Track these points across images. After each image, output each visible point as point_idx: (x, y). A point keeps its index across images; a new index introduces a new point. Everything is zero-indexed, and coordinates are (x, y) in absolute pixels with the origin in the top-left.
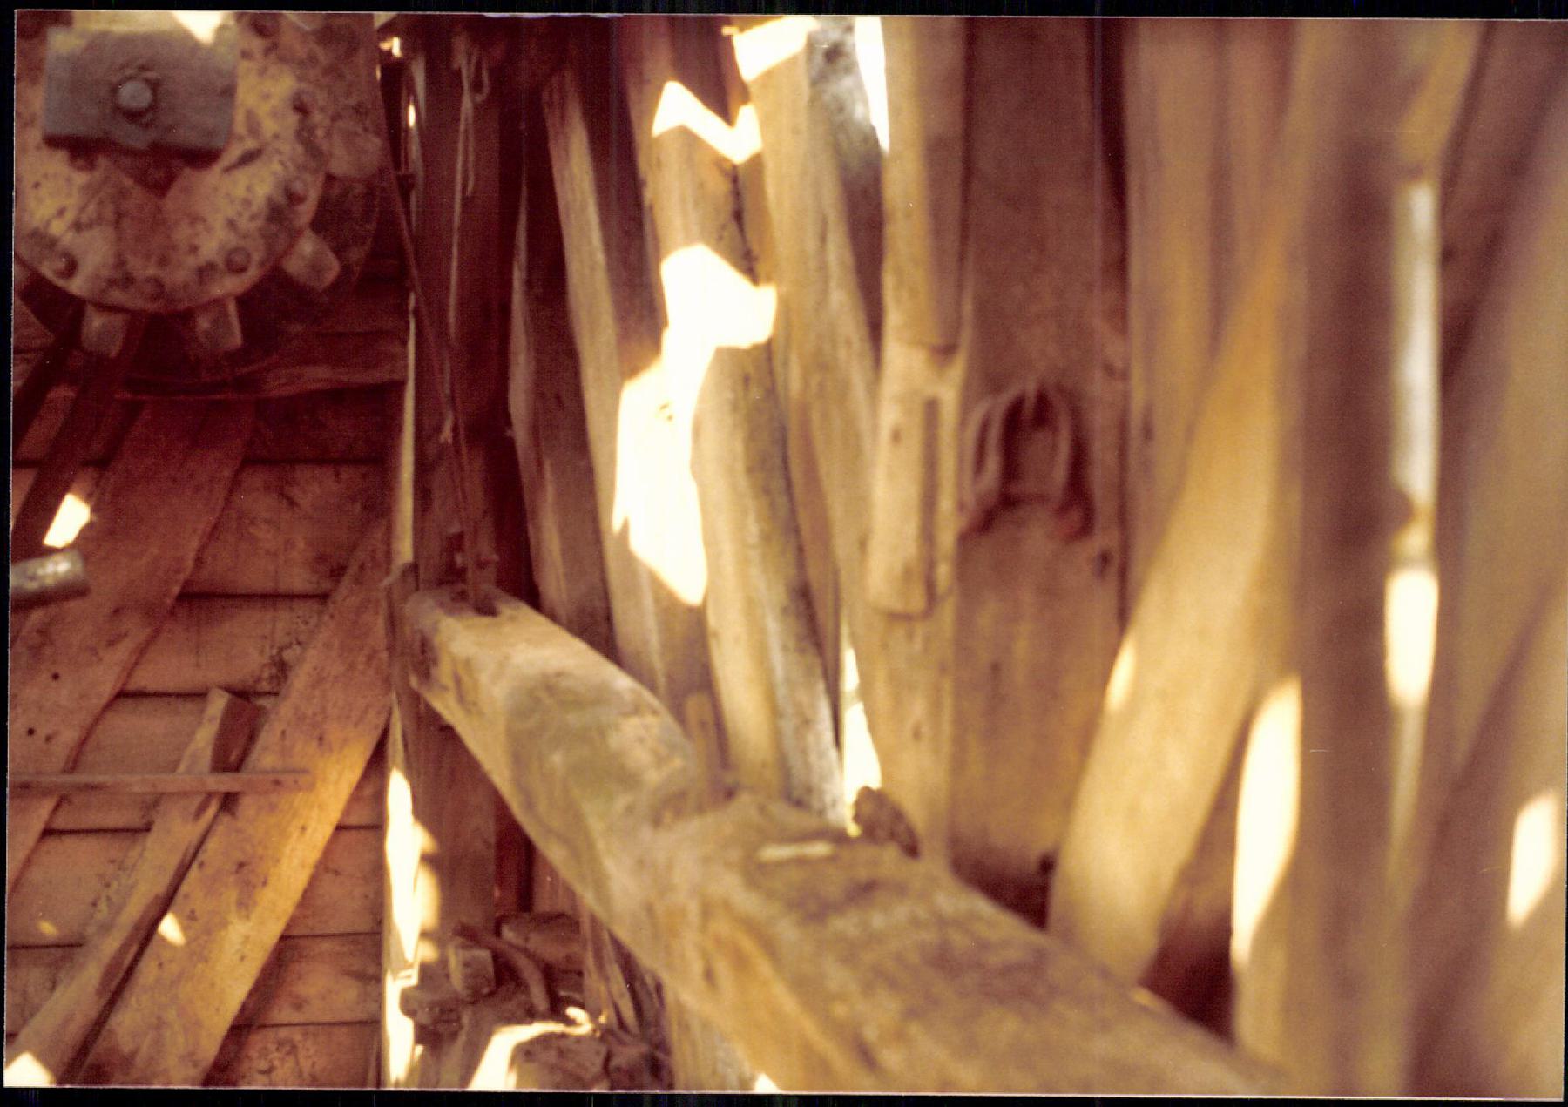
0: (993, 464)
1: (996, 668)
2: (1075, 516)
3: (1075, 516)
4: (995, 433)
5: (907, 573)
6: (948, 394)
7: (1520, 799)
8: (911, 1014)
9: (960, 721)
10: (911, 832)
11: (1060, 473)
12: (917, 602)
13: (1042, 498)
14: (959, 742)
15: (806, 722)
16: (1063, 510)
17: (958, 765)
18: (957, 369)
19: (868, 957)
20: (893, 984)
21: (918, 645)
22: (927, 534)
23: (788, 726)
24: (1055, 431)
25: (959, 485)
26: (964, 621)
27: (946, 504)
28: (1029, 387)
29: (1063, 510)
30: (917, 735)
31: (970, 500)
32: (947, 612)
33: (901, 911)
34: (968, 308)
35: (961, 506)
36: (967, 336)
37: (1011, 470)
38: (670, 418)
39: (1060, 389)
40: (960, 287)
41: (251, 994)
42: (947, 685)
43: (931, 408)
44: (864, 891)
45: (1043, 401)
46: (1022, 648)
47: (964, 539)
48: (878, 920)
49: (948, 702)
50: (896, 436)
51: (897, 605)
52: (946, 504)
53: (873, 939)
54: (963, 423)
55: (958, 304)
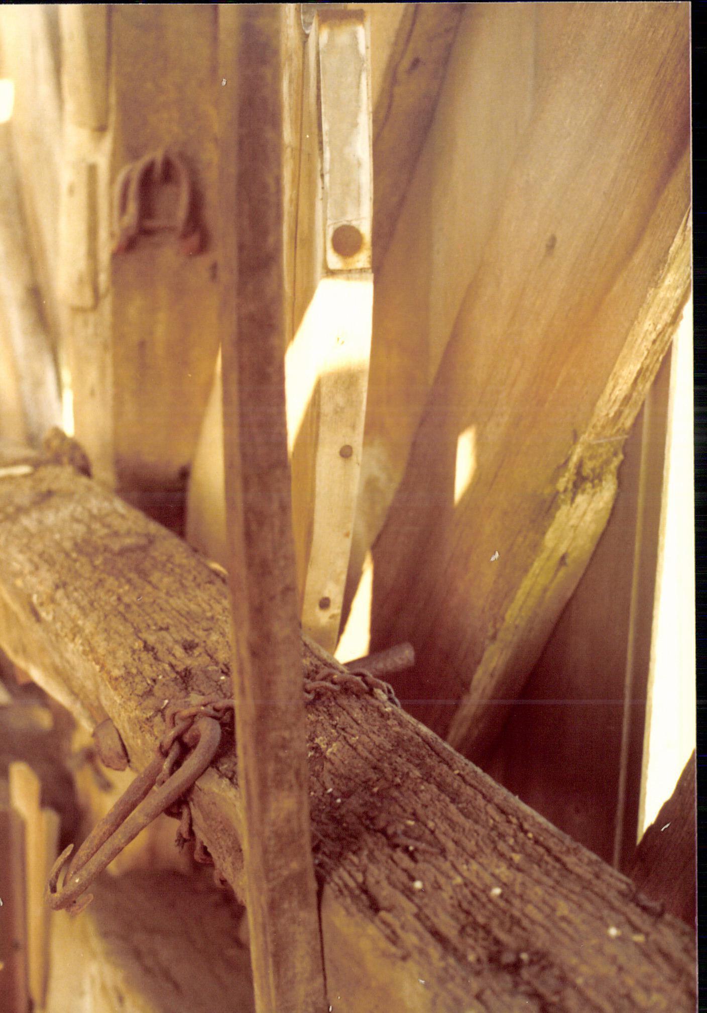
0: (133, 207)
1: (142, 345)
2: (195, 240)
3: (195, 240)
4: (134, 187)
5: (81, 281)
6: (103, 161)
7: (459, 431)
8: (60, 585)
9: (117, 384)
10: (84, 457)
11: (181, 213)
12: (87, 299)
13: (172, 229)
14: (118, 399)
15: (38, 384)
16: (185, 236)
17: (118, 414)
18: (107, 143)
19: (39, 546)
20: (51, 563)
21: (90, 330)
22: (92, 254)
23: (26, 387)
24: (177, 184)
25: (111, 224)
26: (118, 313)
27: (103, 234)
28: (157, 155)
29: (185, 236)
30: (92, 393)
31: (117, 229)
32: (107, 305)
33: (67, 510)
34: (113, 99)
35: (112, 235)
36: (113, 118)
37: (146, 210)
38: (338, 339)
39: (181, 155)
40: (107, 85)
41: (399, 491)
42: (109, 359)
43: (92, 170)
44: (45, 497)
45: (168, 164)
46: (160, 331)
47: (115, 256)
48: (50, 518)
49: (109, 371)
50: (71, 191)
51: (77, 302)
52: (103, 234)
53: (44, 530)
54: (112, 181)
55: (107, 97)
